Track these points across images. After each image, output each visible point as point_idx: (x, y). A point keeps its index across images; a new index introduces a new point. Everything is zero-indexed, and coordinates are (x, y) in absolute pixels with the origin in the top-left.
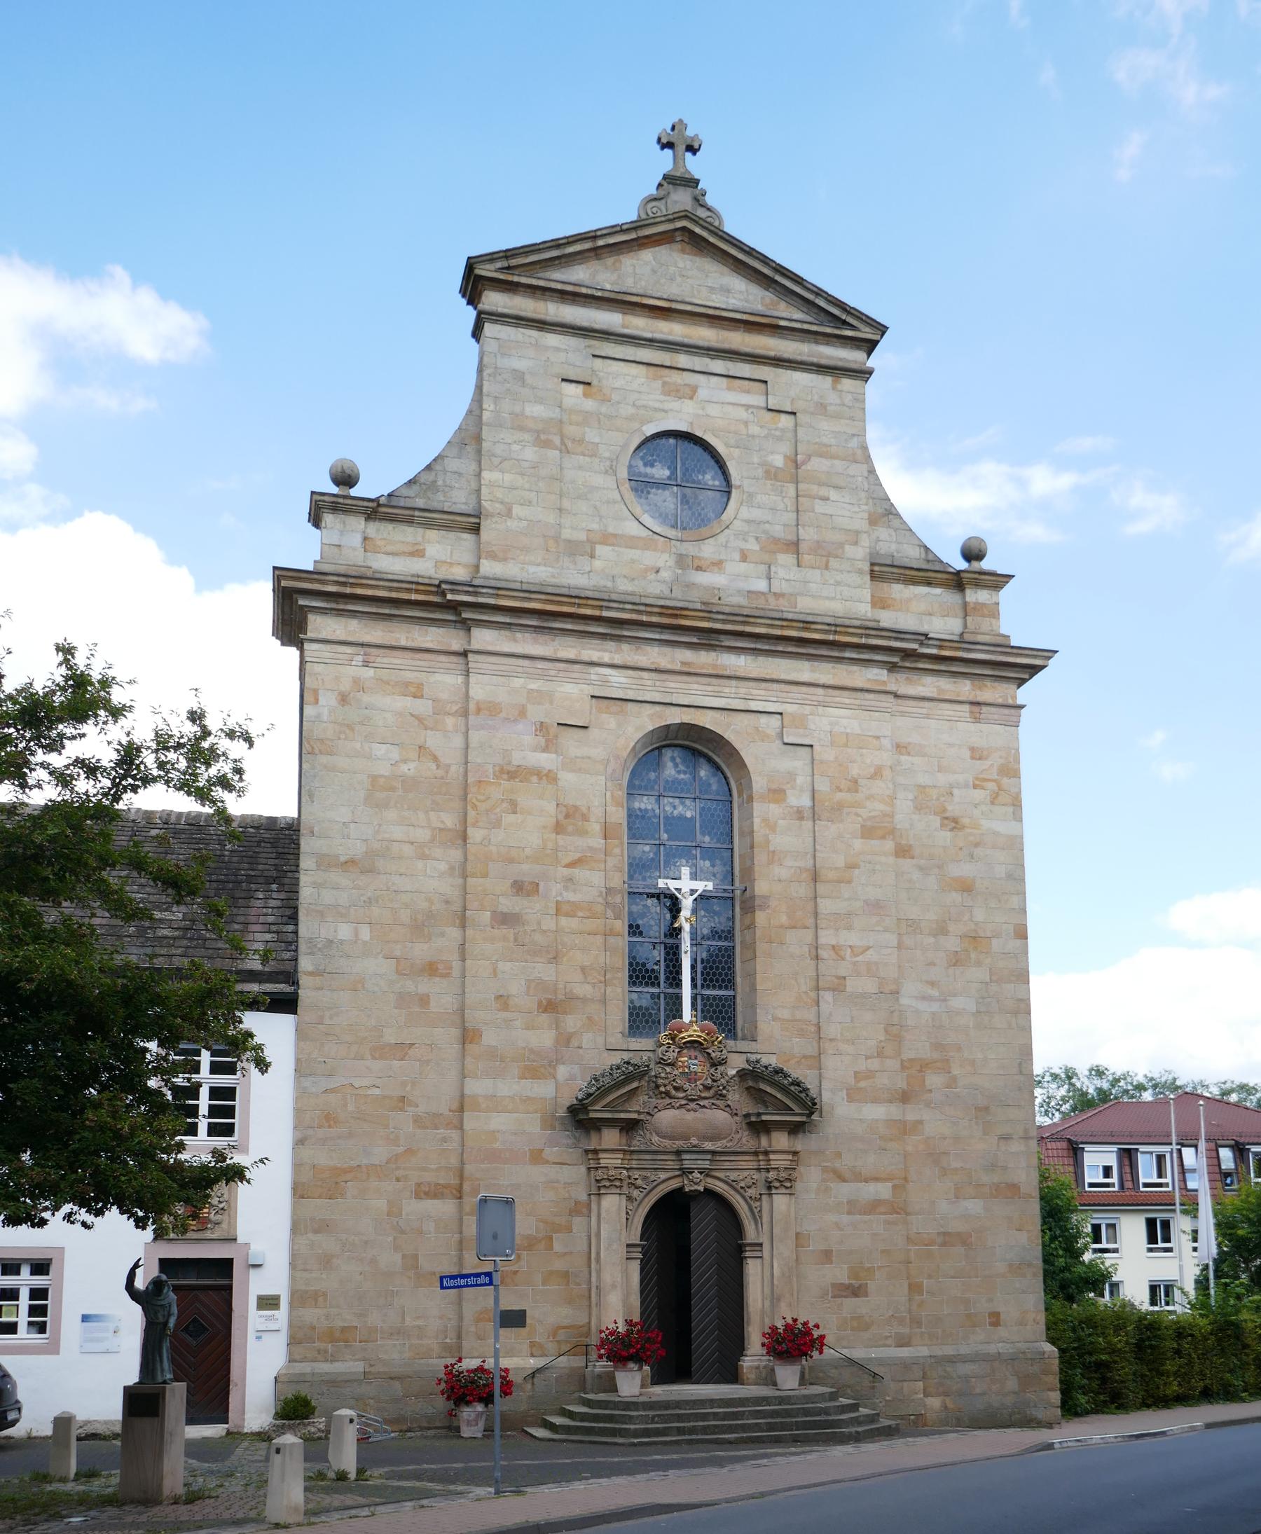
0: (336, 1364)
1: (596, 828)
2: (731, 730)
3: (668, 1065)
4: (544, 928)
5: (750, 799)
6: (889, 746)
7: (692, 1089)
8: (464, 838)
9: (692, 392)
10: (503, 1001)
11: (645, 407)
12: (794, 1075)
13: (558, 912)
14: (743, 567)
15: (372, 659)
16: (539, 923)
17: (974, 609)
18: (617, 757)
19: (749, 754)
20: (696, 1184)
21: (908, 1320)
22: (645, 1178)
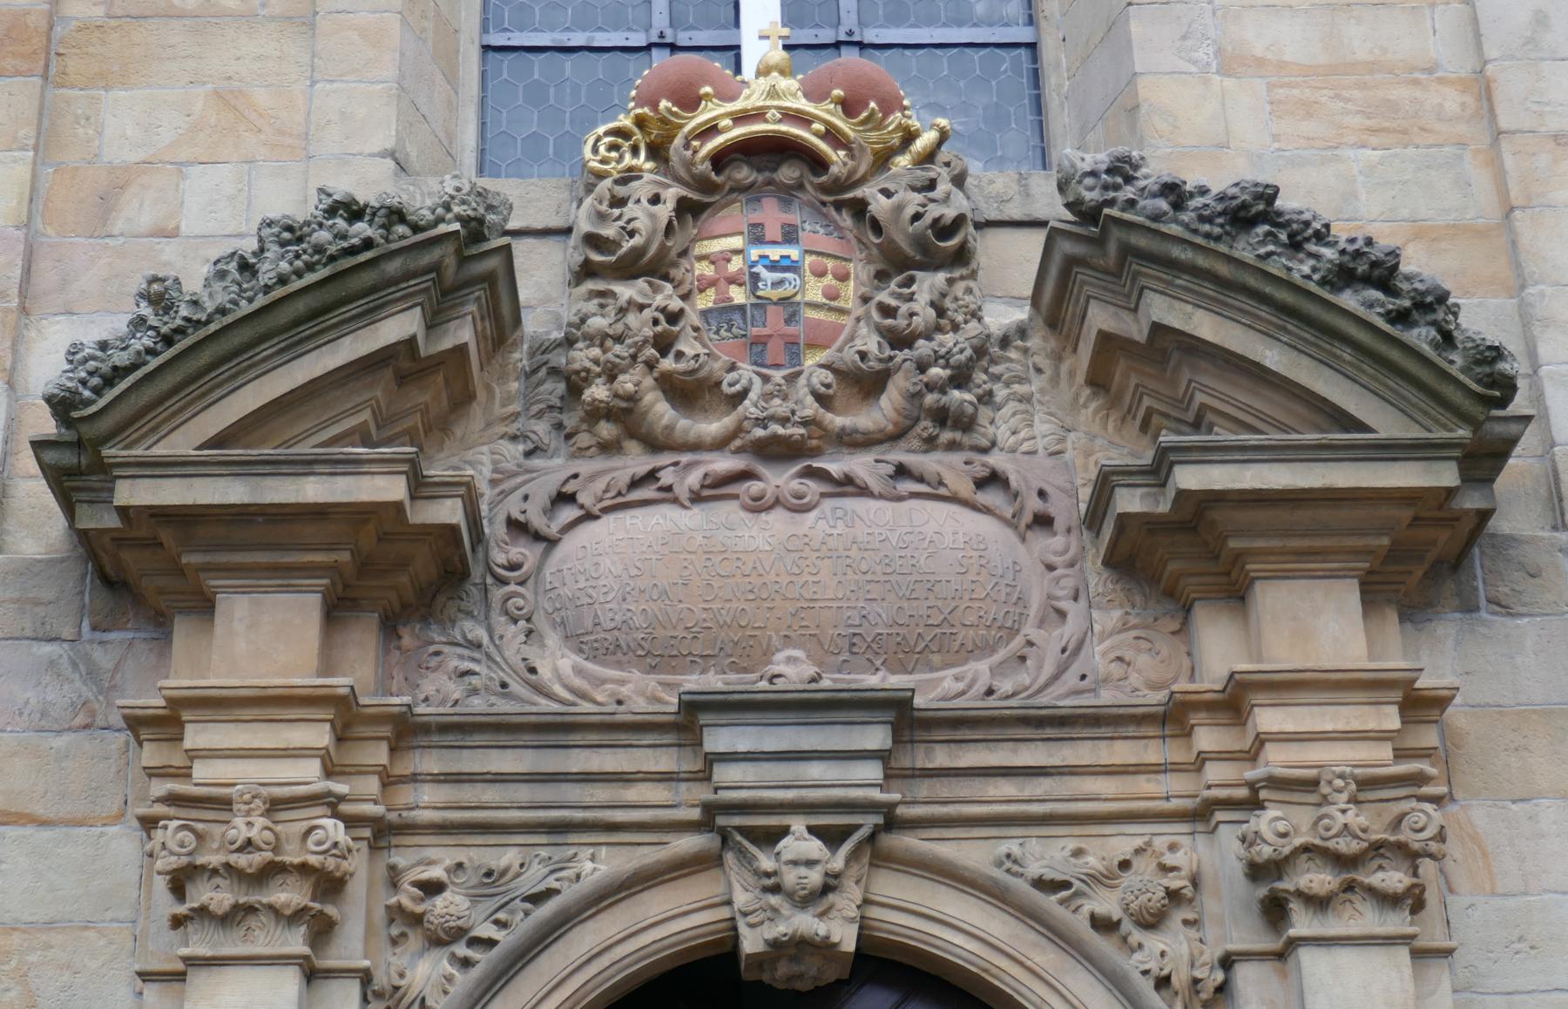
3: (630, 268)
7: (789, 396)
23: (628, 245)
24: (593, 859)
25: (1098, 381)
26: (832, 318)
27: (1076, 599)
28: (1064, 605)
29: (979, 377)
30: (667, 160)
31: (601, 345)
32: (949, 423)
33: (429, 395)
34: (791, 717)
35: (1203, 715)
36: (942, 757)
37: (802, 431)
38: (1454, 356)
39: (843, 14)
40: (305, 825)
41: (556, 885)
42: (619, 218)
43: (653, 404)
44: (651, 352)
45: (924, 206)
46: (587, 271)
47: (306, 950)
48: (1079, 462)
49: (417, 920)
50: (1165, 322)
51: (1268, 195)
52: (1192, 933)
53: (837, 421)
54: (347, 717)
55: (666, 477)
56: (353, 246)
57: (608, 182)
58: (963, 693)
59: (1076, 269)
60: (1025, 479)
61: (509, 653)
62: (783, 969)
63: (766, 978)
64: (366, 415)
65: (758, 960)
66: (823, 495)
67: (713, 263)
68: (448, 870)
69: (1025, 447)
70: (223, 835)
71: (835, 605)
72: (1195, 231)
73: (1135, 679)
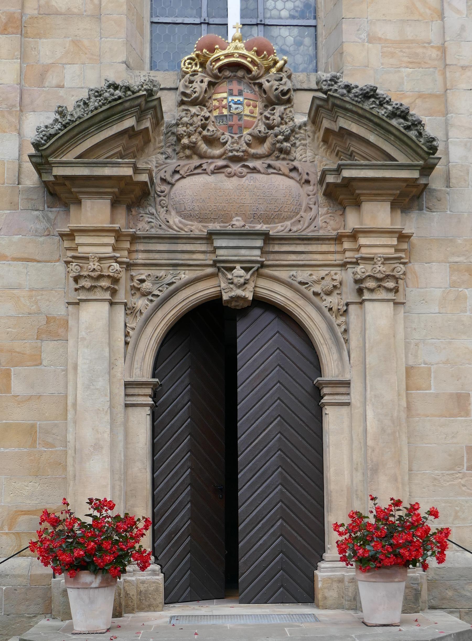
3: (194, 103)
7: (236, 143)
12: (395, 101)
23: (194, 96)
24: (184, 274)
25: (325, 141)
26: (251, 119)
27: (315, 204)
28: (312, 206)
29: (292, 138)
30: (205, 68)
31: (186, 126)
32: (283, 152)
33: (138, 141)
34: (237, 237)
35: (346, 239)
36: (277, 248)
37: (242, 154)
38: (422, 140)
39: (259, 14)
40: (109, 265)
41: (174, 281)
42: (191, 87)
43: (201, 145)
44: (200, 129)
45: (279, 86)
46: (182, 103)
47: (110, 298)
48: (318, 165)
49: (139, 289)
50: (343, 127)
51: (374, 90)
52: (339, 297)
53: (252, 151)
54: (119, 235)
55: (205, 166)
56: (116, 98)
57: (188, 76)
58: (283, 230)
59: (320, 109)
60: (303, 169)
61: (161, 217)
62: (233, 304)
63: (229, 306)
64: (121, 148)
65: (227, 301)
66: (248, 173)
67: (218, 101)
68: (146, 276)
69: (304, 160)
70: (87, 267)
71: (250, 205)
72: (353, 100)
73: (329, 228)
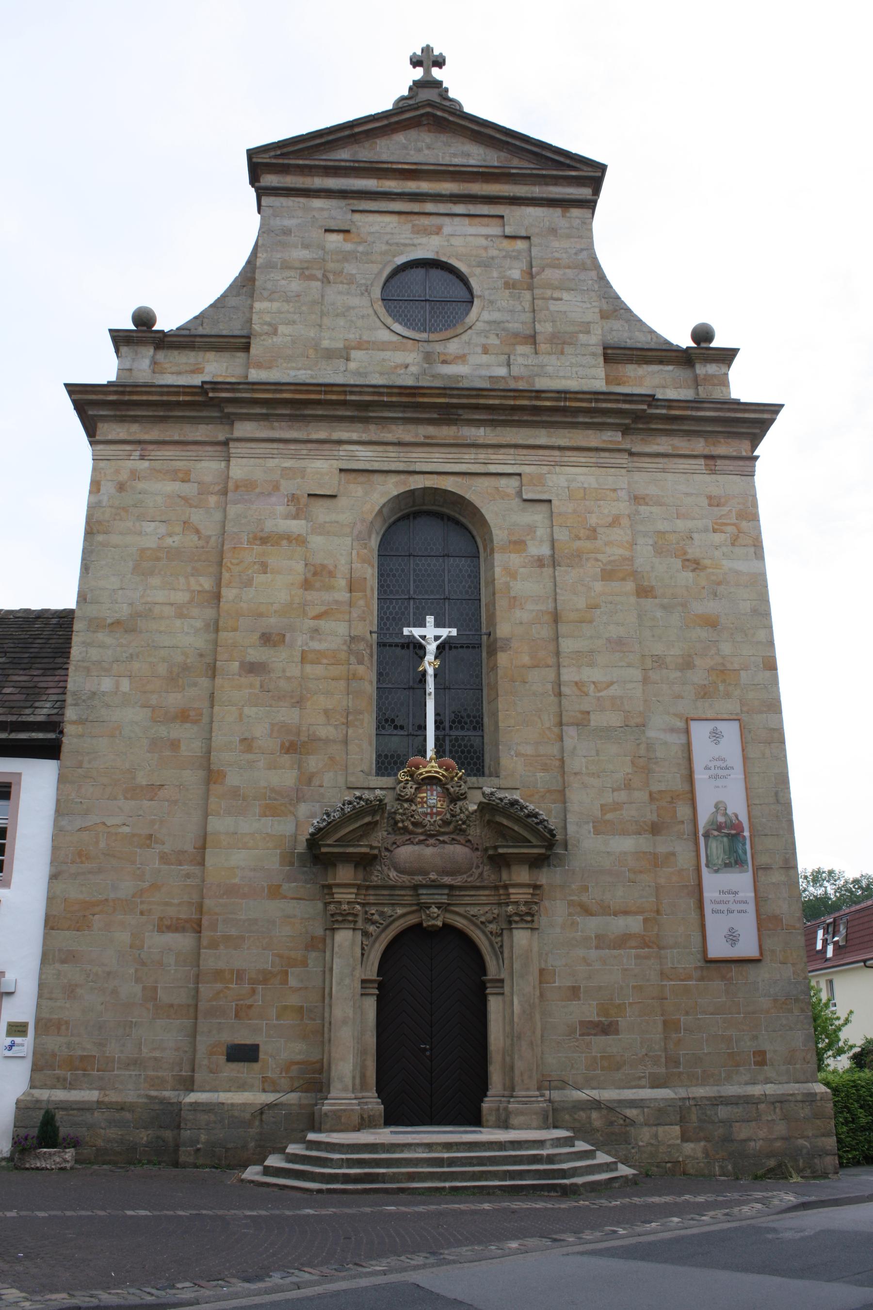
0: (74, 1092)
1: (343, 583)
2: (475, 492)
3: (407, 801)
4: (288, 674)
5: (492, 551)
6: (627, 498)
8: (218, 596)
9: (438, 231)
10: (247, 744)
11: (397, 244)
13: (303, 660)
14: (485, 358)
15: (147, 453)
16: (284, 671)
17: (705, 379)
18: (363, 521)
19: (490, 511)
20: (434, 919)
21: (663, 1060)
22: (381, 914)
49: (370, 920)
53: (442, 830)
62: (430, 929)
